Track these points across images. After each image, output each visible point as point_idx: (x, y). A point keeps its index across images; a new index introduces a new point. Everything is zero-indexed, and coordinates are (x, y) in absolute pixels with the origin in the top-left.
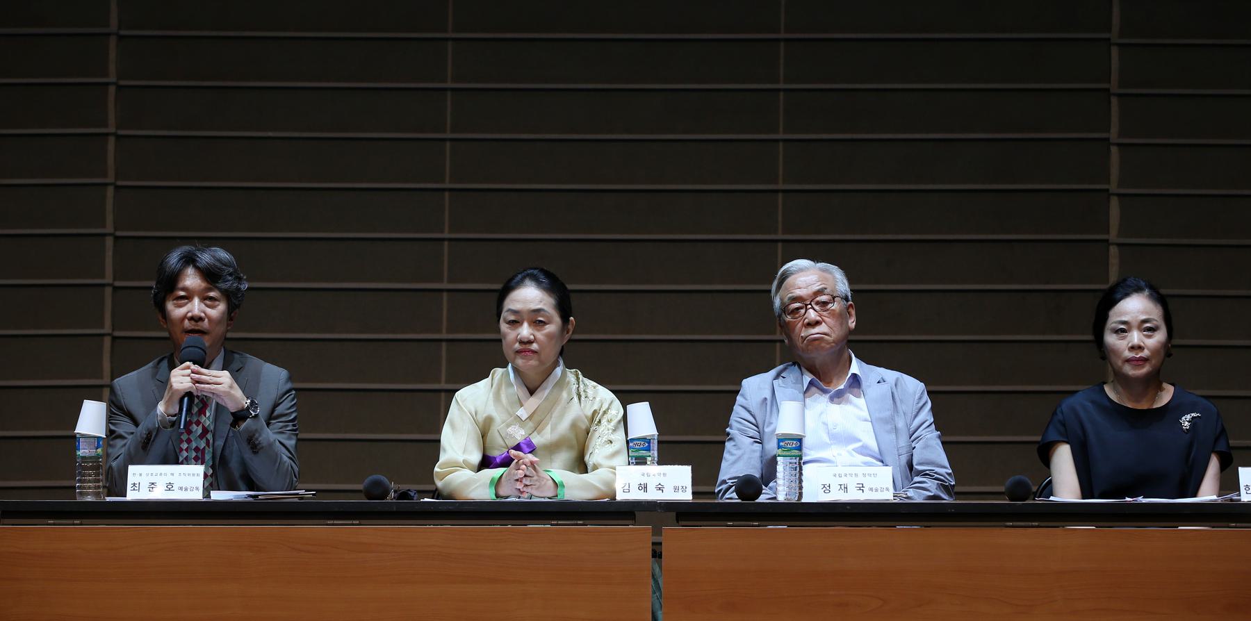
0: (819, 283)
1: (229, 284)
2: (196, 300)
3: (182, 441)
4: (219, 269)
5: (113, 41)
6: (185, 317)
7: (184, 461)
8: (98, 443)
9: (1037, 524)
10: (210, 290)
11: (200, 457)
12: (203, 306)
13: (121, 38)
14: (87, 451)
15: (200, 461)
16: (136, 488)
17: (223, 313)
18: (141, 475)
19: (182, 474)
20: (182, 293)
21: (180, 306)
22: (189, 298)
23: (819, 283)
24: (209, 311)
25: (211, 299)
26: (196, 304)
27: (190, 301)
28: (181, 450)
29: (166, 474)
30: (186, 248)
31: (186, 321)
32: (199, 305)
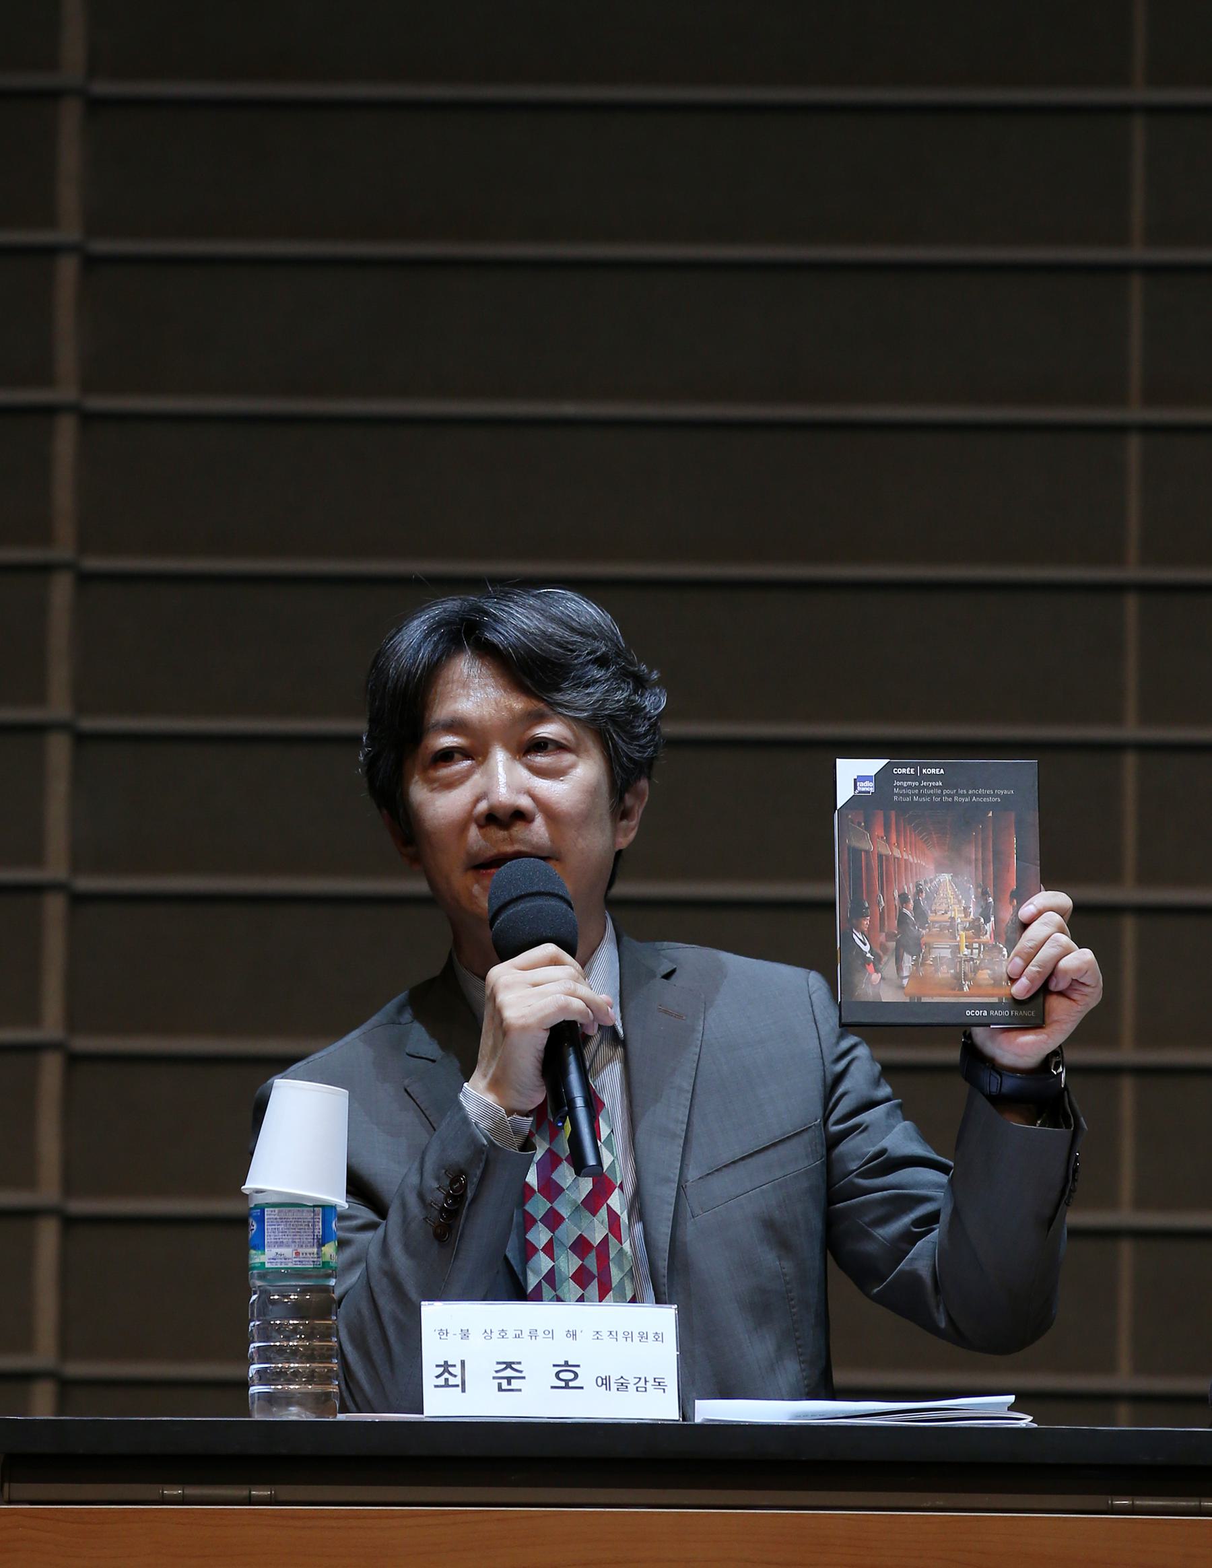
0: (396, 643)
1: (597, 692)
2: (500, 758)
3: (529, 1222)
4: (559, 645)
5: (70, 118)
6: (469, 818)
7: (546, 1287)
8: (326, 1223)
9: (266, 1493)
10: (540, 719)
11: (595, 1270)
12: (524, 773)
13: (95, 106)
14: (288, 1252)
15: (594, 1288)
16: (452, 1381)
17: (593, 792)
18: (465, 1334)
19: (605, 1334)
20: (448, 741)
21: (450, 785)
22: (476, 753)
23: (396, 643)
24: (545, 787)
25: (541, 745)
26: (501, 770)
27: (481, 764)
28: (528, 1251)
29: (550, 1334)
30: (450, 605)
31: (474, 832)
32: (508, 771)
